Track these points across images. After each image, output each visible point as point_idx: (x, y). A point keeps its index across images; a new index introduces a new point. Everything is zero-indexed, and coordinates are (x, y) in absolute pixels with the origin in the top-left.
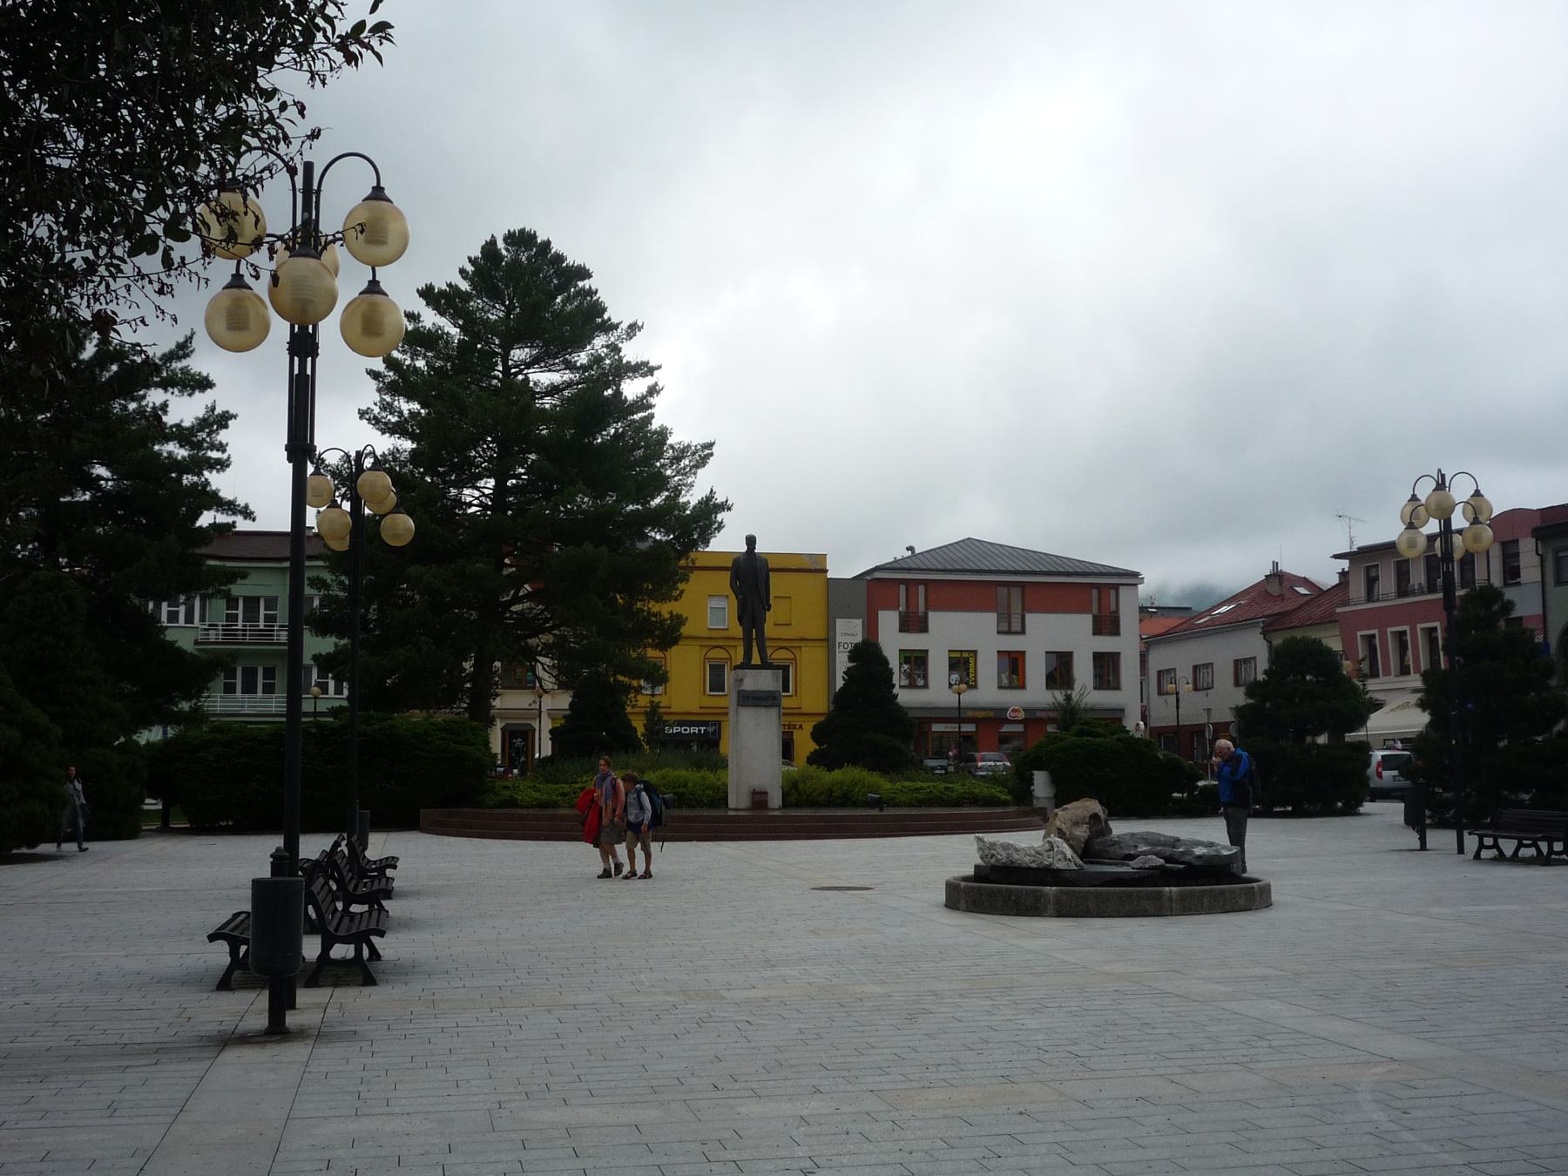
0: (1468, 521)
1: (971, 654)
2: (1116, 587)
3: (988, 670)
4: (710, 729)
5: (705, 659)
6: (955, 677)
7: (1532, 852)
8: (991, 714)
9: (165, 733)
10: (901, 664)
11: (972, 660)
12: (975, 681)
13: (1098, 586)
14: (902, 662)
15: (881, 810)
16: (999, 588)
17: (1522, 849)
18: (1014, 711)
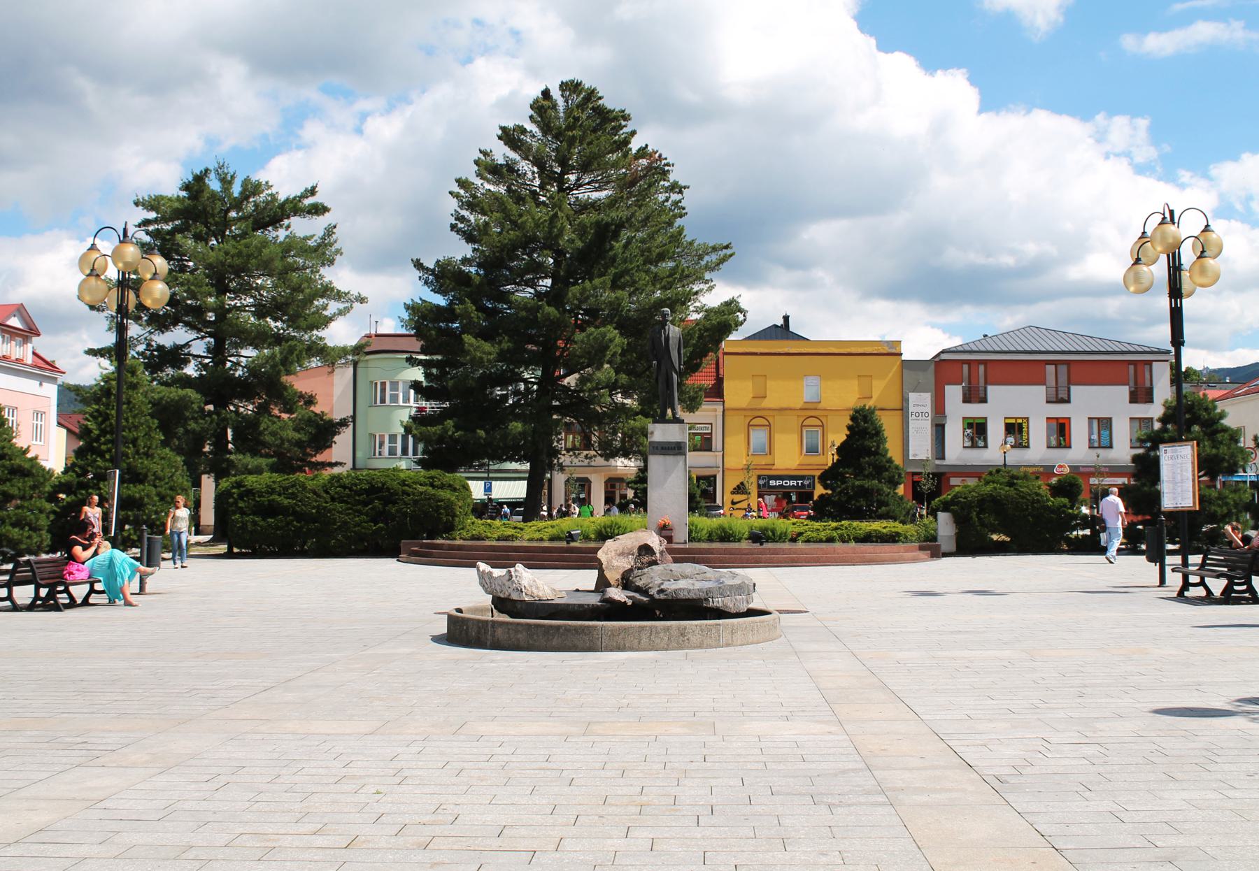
0: (1196, 255)
1: (1025, 421)
2: (1150, 363)
3: (1038, 433)
4: (806, 483)
5: (802, 426)
6: (1011, 439)
7: (1201, 592)
8: (1041, 470)
9: (488, 489)
10: (964, 429)
11: (1025, 425)
12: (1028, 442)
13: (1135, 363)
14: (966, 426)
15: (761, 544)
16: (1047, 366)
17: (93, 595)
18: (1060, 466)
